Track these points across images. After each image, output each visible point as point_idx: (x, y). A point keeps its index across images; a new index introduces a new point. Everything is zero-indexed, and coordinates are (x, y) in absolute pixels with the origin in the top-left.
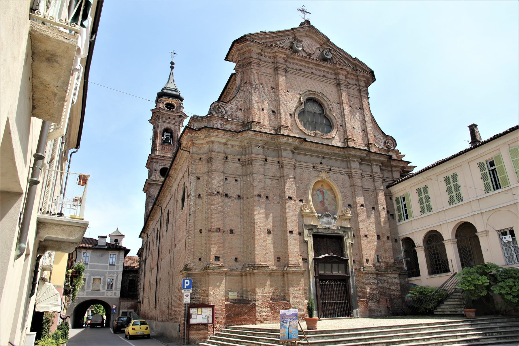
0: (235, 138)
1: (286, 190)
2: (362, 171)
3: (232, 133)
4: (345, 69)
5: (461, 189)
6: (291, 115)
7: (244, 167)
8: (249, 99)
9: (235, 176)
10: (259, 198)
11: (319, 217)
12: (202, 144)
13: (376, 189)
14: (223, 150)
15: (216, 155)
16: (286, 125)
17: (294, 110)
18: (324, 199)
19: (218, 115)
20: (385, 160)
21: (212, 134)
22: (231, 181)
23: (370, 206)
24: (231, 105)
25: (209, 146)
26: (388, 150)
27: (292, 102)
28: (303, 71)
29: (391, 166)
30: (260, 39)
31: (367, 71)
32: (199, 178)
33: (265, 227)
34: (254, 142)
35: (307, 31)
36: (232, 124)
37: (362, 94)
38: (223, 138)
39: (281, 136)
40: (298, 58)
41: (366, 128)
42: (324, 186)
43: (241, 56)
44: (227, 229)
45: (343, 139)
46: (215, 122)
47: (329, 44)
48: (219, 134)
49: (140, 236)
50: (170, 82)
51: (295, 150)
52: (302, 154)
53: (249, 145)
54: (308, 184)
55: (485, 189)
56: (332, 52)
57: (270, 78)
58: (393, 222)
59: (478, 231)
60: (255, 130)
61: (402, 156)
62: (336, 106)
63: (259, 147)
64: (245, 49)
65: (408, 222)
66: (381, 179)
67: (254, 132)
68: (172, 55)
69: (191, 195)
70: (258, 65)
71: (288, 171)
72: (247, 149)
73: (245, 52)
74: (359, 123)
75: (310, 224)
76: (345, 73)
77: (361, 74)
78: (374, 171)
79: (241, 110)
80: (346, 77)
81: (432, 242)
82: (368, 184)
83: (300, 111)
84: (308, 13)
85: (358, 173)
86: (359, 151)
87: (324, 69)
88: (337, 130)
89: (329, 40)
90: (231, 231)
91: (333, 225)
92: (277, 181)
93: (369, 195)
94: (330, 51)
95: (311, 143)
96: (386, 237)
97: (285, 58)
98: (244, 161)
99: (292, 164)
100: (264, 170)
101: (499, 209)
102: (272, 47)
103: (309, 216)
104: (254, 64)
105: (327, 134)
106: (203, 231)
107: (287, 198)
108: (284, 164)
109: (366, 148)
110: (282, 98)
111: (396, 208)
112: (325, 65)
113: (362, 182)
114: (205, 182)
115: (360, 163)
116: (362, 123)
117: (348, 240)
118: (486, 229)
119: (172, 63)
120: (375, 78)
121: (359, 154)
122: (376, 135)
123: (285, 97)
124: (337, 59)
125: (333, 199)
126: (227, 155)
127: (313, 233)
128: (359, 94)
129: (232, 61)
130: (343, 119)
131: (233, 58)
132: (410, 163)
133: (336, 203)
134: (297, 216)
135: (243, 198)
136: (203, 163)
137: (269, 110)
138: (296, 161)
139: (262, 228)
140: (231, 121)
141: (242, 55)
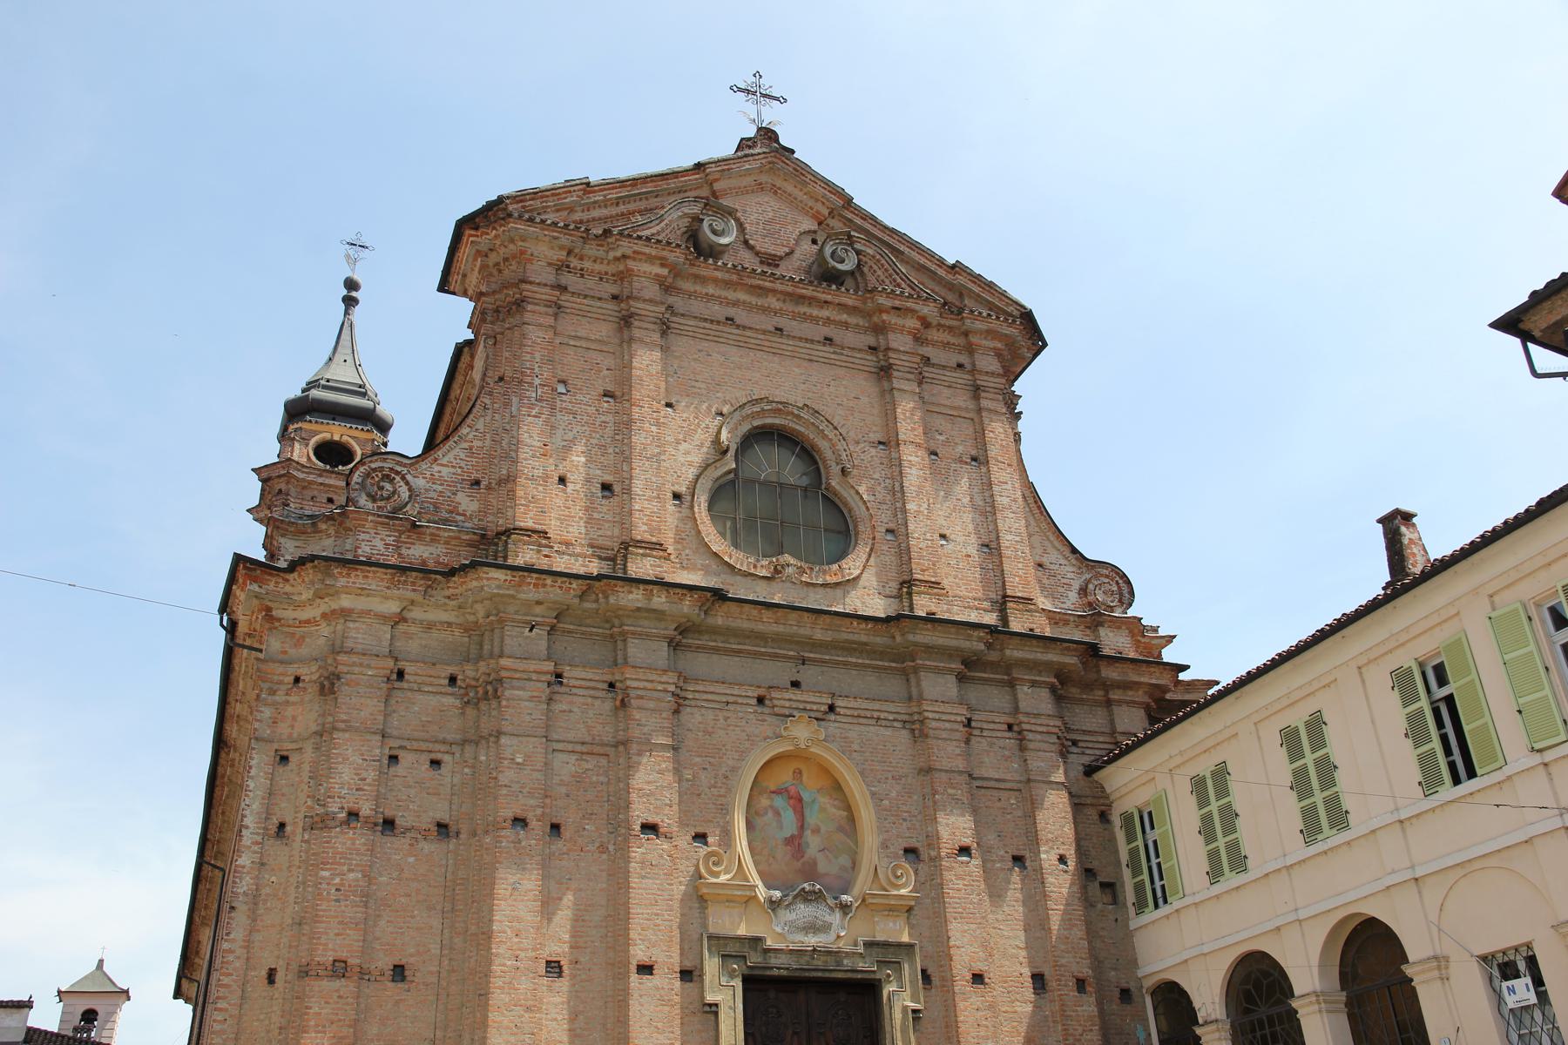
0: (439, 595)
1: (634, 796)
2: (970, 709)
3: (423, 578)
4: (912, 311)
5: (1288, 779)
6: (677, 496)
7: (470, 711)
8: (510, 443)
9: (431, 746)
10: (518, 834)
11: (774, 905)
12: (308, 622)
13: (1029, 780)
14: (386, 643)
15: (354, 664)
16: (654, 540)
17: (691, 477)
18: (802, 827)
19: (379, 507)
20: (1071, 660)
21: (342, 582)
22: (413, 765)
23: (1003, 854)
24: (436, 468)
25: (332, 629)
26: (1095, 618)
27: (684, 446)
28: (738, 327)
29: (1107, 686)
30: (566, 209)
31: (1005, 313)
32: (284, 759)
33: (534, 949)
34: (511, 609)
35: (761, 170)
36: (435, 539)
37: (984, 403)
38: (387, 598)
39: (620, 583)
40: (719, 274)
41: (998, 538)
42: (805, 778)
43: (491, 275)
44: (380, 964)
45: (894, 585)
46: (363, 536)
47: (850, 216)
48: (370, 581)
49: (178, 994)
50: (339, 358)
51: (682, 638)
52: (716, 650)
53: (491, 623)
54: (734, 770)
55: (1421, 779)
56: (857, 246)
57: (599, 357)
58: (1112, 917)
59: (1410, 960)
60: (520, 561)
61: (1164, 641)
62: (870, 456)
63: (531, 630)
64: (502, 250)
65: (1167, 917)
66: (1054, 739)
67: (509, 572)
68: (351, 252)
69: (247, 827)
70: (550, 311)
71: (649, 721)
72: (487, 636)
73: (506, 260)
74: (968, 517)
75: (731, 933)
76: (912, 323)
77: (979, 325)
78: (1022, 705)
79: (477, 483)
80: (917, 339)
81: (1257, 1005)
82: (995, 759)
83: (717, 485)
84: (776, 99)
85: (953, 718)
86: (953, 630)
87: (825, 313)
88: (871, 550)
89: (848, 201)
90: (399, 972)
91: (834, 936)
92: (603, 761)
93: (999, 804)
94: (851, 244)
95: (747, 607)
96: (1072, 983)
97: (666, 277)
98: (473, 683)
99: (665, 691)
100: (548, 719)
101: (1476, 865)
102: (610, 240)
103: (730, 900)
104: (537, 308)
105: (826, 567)
106: (279, 977)
107: (638, 828)
108: (633, 693)
109: (991, 619)
110: (644, 435)
111: (1124, 857)
112: (829, 298)
113: (967, 755)
114: (305, 775)
115: (961, 678)
116: (979, 519)
117: (900, 998)
118: (1438, 946)
119: (351, 285)
120: (1041, 337)
121: (954, 643)
122: (1045, 560)
123: (654, 428)
124: (879, 273)
125: (840, 829)
126: (401, 664)
127: (746, 972)
128: (971, 405)
129: (465, 294)
130: (898, 505)
131: (467, 281)
132: (1185, 668)
133: (856, 843)
134: (676, 905)
135: (458, 834)
136: (307, 698)
137: (588, 480)
138: (686, 680)
139: (522, 954)
140: (428, 531)
141: (495, 272)
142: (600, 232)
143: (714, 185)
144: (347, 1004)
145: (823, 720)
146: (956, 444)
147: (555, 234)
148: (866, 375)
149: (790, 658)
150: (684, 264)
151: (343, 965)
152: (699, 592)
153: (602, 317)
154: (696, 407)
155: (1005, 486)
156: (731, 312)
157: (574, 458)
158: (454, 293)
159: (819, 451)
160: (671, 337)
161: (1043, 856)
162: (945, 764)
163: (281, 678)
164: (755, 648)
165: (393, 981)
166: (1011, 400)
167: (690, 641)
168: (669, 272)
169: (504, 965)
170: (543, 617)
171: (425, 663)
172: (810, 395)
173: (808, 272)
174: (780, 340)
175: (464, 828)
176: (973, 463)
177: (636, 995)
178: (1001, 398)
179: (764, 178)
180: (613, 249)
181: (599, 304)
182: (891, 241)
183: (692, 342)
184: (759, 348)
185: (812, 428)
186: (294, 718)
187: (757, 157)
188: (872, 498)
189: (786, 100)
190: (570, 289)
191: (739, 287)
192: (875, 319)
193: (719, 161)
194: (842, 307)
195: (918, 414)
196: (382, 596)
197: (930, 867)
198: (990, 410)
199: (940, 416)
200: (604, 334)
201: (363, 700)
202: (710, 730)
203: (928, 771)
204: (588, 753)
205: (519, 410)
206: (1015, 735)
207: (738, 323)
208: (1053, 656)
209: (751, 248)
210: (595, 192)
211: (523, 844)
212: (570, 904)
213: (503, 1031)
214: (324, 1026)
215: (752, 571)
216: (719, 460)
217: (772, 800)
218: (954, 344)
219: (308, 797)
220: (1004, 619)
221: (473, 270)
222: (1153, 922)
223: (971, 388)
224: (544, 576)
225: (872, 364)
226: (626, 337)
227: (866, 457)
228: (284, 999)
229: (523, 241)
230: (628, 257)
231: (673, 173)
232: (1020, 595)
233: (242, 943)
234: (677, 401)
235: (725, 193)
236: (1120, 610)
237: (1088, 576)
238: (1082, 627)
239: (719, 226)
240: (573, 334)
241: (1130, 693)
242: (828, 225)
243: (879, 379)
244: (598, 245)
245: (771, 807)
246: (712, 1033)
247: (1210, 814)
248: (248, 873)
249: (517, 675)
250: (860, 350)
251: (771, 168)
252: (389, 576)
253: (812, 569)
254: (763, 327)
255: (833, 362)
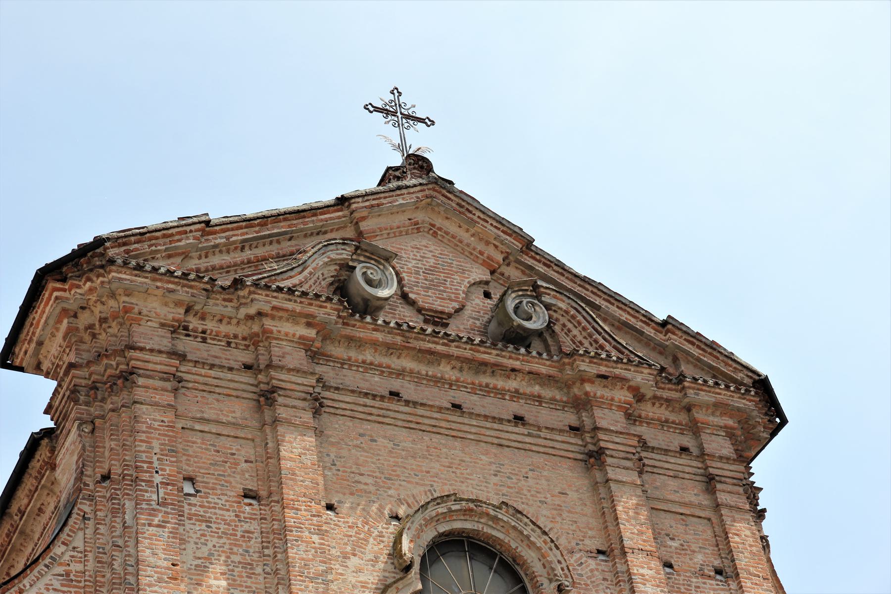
4: (623, 380)
8: (125, 564)
27: (354, 562)
28: (407, 403)
31: (734, 381)
37: (722, 497)
40: (379, 336)
43: (81, 341)
47: (530, 262)
57: (234, 446)
70: (168, 385)
73: (102, 320)
76: (622, 395)
80: (632, 417)
87: (512, 384)
89: (528, 243)
94: (538, 297)
97: (313, 341)
102: (241, 293)
112: (517, 364)
120: (780, 413)
123: (315, 538)
124: (575, 332)
128: (704, 500)
129: (37, 369)
141: (87, 337)
142: (228, 283)
143: (361, 224)
146: (694, 551)
147: (171, 286)
148: (569, 463)
150: (336, 323)
153: (234, 393)
154: (364, 509)
157: (212, 582)
158: (21, 369)
159: (524, 564)
166: (752, 492)
168: (318, 333)
172: (505, 490)
173: (484, 333)
174: (460, 420)
176: (718, 577)
178: (741, 490)
179: (420, 216)
180: (245, 304)
181: (229, 376)
182: (583, 293)
183: (351, 424)
184: (435, 430)
185: (513, 534)
187: (412, 190)
189: (433, 123)
190: (189, 357)
191: (405, 352)
192: (576, 390)
193: (367, 194)
194: (533, 375)
195: (644, 514)
198: (731, 507)
199: (668, 515)
200: (238, 414)
205: (135, 517)
207: (405, 397)
209: (412, 303)
210: (215, 233)
216: (401, 579)
218: (673, 422)
221: (53, 335)
223: (704, 479)
227: (584, 571)
229: (128, 295)
230: (266, 315)
231: (312, 209)
234: (340, 502)
235: (374, 234)
239: (375, 276)
240: (198, 416)
242: (503, 274)
243: (588, 468)
244: (224, 300)
250: (561, 431)
254: (437, 403)
255: (527, 446)
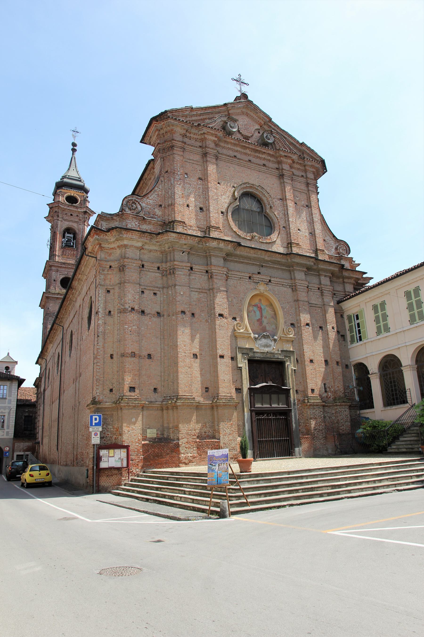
0: (154, 241)
1: (216, 306)
2: (309, 283)
3: (149, 236)
4: (290, 157)
6: (222, 213)
7: (164, 278)
9: (153, 289)
10: (183, 316)
11: (256, 339)
12: (113, 248)
13: (324, 305)
15: (129, 262)
17: (226, 207)
18: (262, 316)
19: (132, 212)
21: (125, 236)
23: (317, 326)
24: (148, 200)
26: (341, 258)
27: (224, 197)
28: (238, 159)
29: (344, 278)
31: (316, 160)
32: (108, 291)
33: (190, 350)
34: (177, 246)
36: (150, 223)
37: (310, 188)
40: (232, 141)
41: (314, 231)
43: (161, 137)
44: (144, 354)
45: (285, 244)
46: (128, 221)
47: (270, 125)
49: (37, 363)
50: (71, 169)
52: (236, 262)
53: (170, 250)
54: (243, 298)
56: (274, 135)
57: (197, 166)
61: (357, 265)
62: (278, 203)
63: (183, 253)
64: (165, 129)
66: (331, 293)
67: (177, 234)
68: (74, 134)
69: (100, 312)
70: (182, 150)
71: (219, 282)
73: (166, 132)
74: (305, 224)
75: (244, 347)
76: (290, 161)
77: (309, 163)
79: (161, 206)
80: (291, 167)
81: (389, 369)
82: (315, 298)
83: (234, 209)
84: (246, 84)
85: (304, 285)
87: (263, 156)
88: (279, 232)
90: (149, 356)
92: (206, 295)
93: (316, 311)
94: (272, 134)
98: (165, 269)
99: (223, 273)
102: (200, 127)
103: (243, 337)
106: (115, 356)
108: (214, 274)
109: (313, 255)
112: (265, 151)
116: (309, 225)
119: (74, 145)
120: (326, 169)
121: (305, 262)
122: (326, 239)
125: (272, 317)
126: (144, 263)
128: (306, 189)
129: (150, 144)
130: (287, 219)
131: (151, 139)
132: (365, 273)
133: (277, 321)
134: (229, 338)
135: (163, 316)
136: (114, 273)
138: (229, 270)
140: (148, 220)
141: (162, 137)
144: (136, 365)
145: (267, 284)
147: (183, 124)
149: (258, 265)
151: (134, 354)
152: (234, 243)
155: (316, 215)
156: (236, 154)
159: (263, 200)
160: (218, 161)
161: (328, 327)
162: (302, 299)
163: (106, 266)
164: (248, 262)
165: (148, 359)
167: (229, 258)
169: (182, 355)
170: (186, 249)
171: (150, 263)
172: (260, 182)
174: (250, 164)
175: (166, 314)
177: (219, 364)
178: (315, 187)
180: (201, 130)
181: (196, 149)
185: (261, 193)
186: (111, 279)
187: (243, 103)
188: (279, 216)
189: (249, 85)
192: (279, 159)
196: (137, 241)
197: (298, 329)
200: (198, 159)
201: (133, 274)
202: (236, 286)
203: (298, 300)
204: (201, 292)
206: (320, 291)
208: (332, 268)
209: (240, 133)
211: (185, 319)
212: (198, 337)
213: (182, 373)
214: (130, 371)
215: (245, 237)
217: (253, 308)
219: (118, 303)
220: (317, 255)
222: (356, 346)
224: (187, 236)
225: (277, 174)
226: (205, 160)
228: (117, 363)
229: (172, 126)
230: (205, 134)
232: (321, 249)
233: (102, 347)
236: (346, 255)
237: (338, 244)
238: (336, 260)
241: (350, 280)
242: (263, 127)
243: (280, 179)
244: (196, 129)
245: (253, 310)
246: (240, 375)
247: (378, 316)
248: (101, 326)
249: (180, 267)
250: (274, 169)
251: (247, 107)
252: (139, 234)
253: (262, 238)
255: (266, 172)
